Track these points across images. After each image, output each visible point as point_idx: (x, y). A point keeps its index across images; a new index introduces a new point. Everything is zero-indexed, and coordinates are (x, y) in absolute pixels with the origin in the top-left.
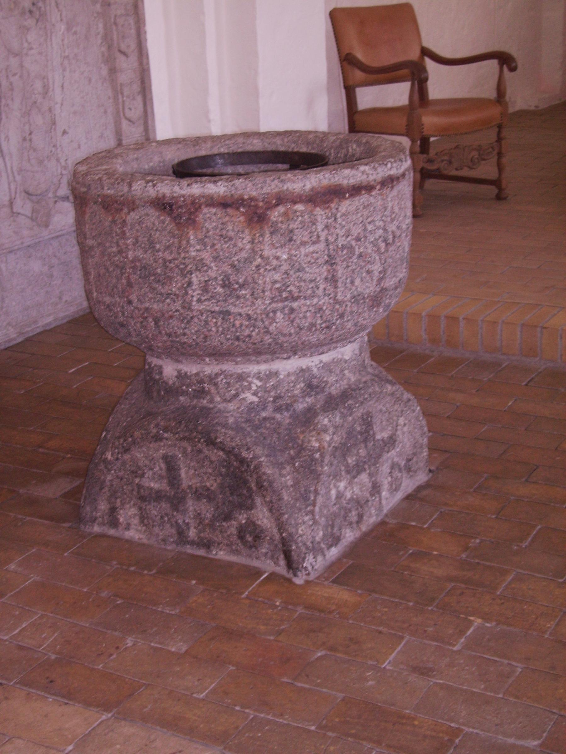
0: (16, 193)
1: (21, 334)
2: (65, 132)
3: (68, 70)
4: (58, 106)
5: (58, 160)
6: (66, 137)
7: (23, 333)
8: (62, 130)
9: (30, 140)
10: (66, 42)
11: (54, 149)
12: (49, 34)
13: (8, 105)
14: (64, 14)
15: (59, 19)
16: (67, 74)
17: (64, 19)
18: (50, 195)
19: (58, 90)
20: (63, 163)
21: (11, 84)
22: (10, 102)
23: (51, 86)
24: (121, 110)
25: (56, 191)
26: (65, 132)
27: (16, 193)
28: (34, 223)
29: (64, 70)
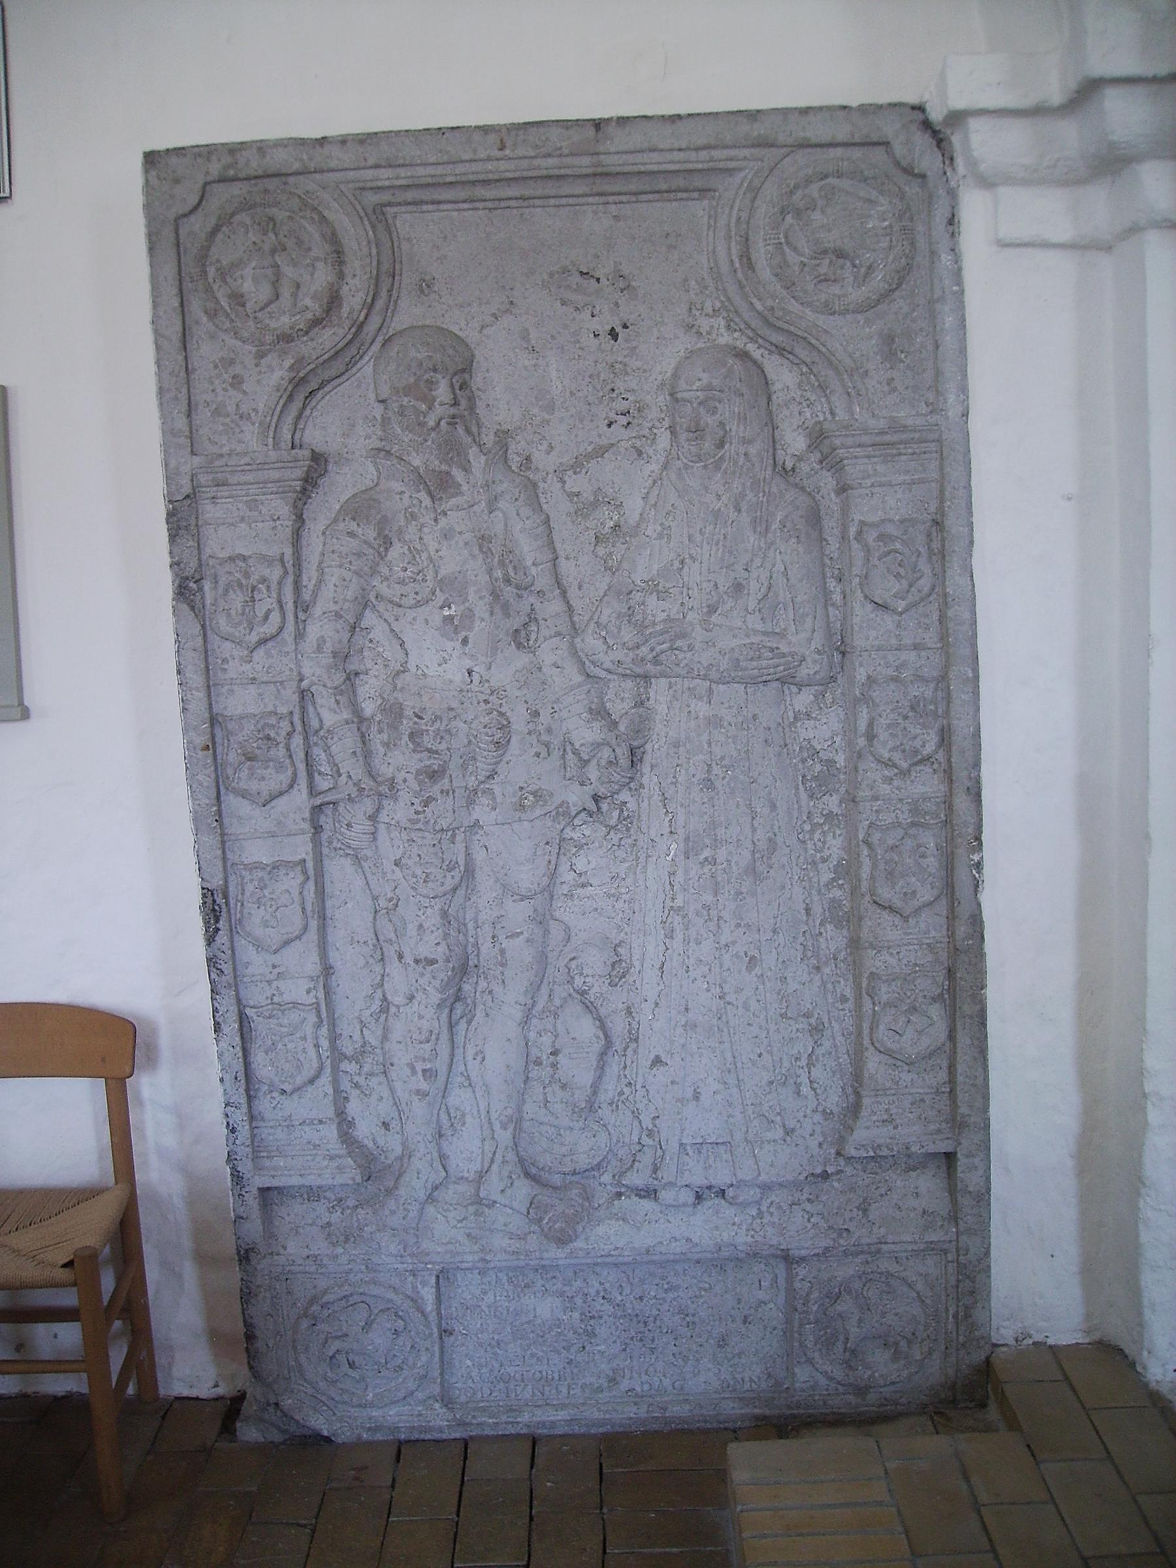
0: (492, 1161)
1: (462, 1424)
2: (657, 1061)
3: (679, 935)
4: (647, 1007)
5: (636, 1114)
6: (659, 1071)
7: (466, 1424)
8: (652, 1057)
9: (554, 1066)
10: (680, 877)
11: (627, 1091)
12: (642, 860)
13: (490, 992)
14: (681, 819)
15: (666, 830)
16: (677, 943)
17: (681, 831)
18: (606, 1178)
19: (651, 975)
20: (647, 1123)
21: (502, 952)
22: (497, 989)
23: (637, 964)
24: (866, 1032)
25: (622, 1174)
26: (657, 1061)
27: (492, 1161)
28: (535, 1228)
29: (670, 935)
